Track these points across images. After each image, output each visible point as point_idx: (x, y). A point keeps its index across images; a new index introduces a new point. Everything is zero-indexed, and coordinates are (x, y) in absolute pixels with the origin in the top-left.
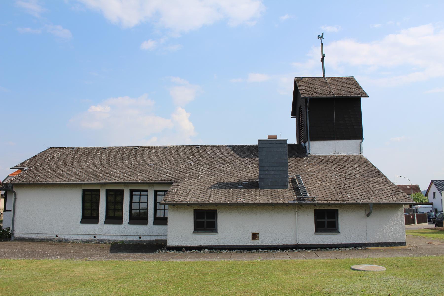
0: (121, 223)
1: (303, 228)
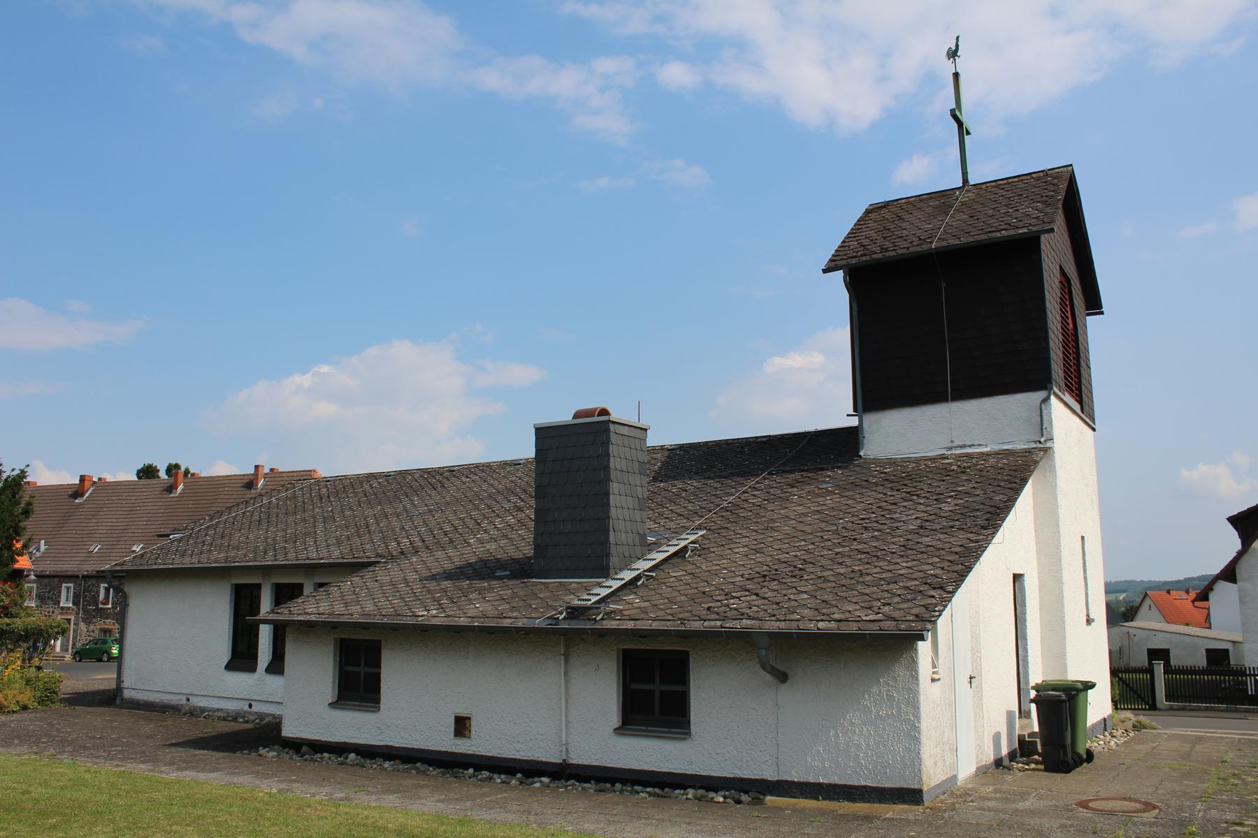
0: (253, 669)
1: (577, 713)
